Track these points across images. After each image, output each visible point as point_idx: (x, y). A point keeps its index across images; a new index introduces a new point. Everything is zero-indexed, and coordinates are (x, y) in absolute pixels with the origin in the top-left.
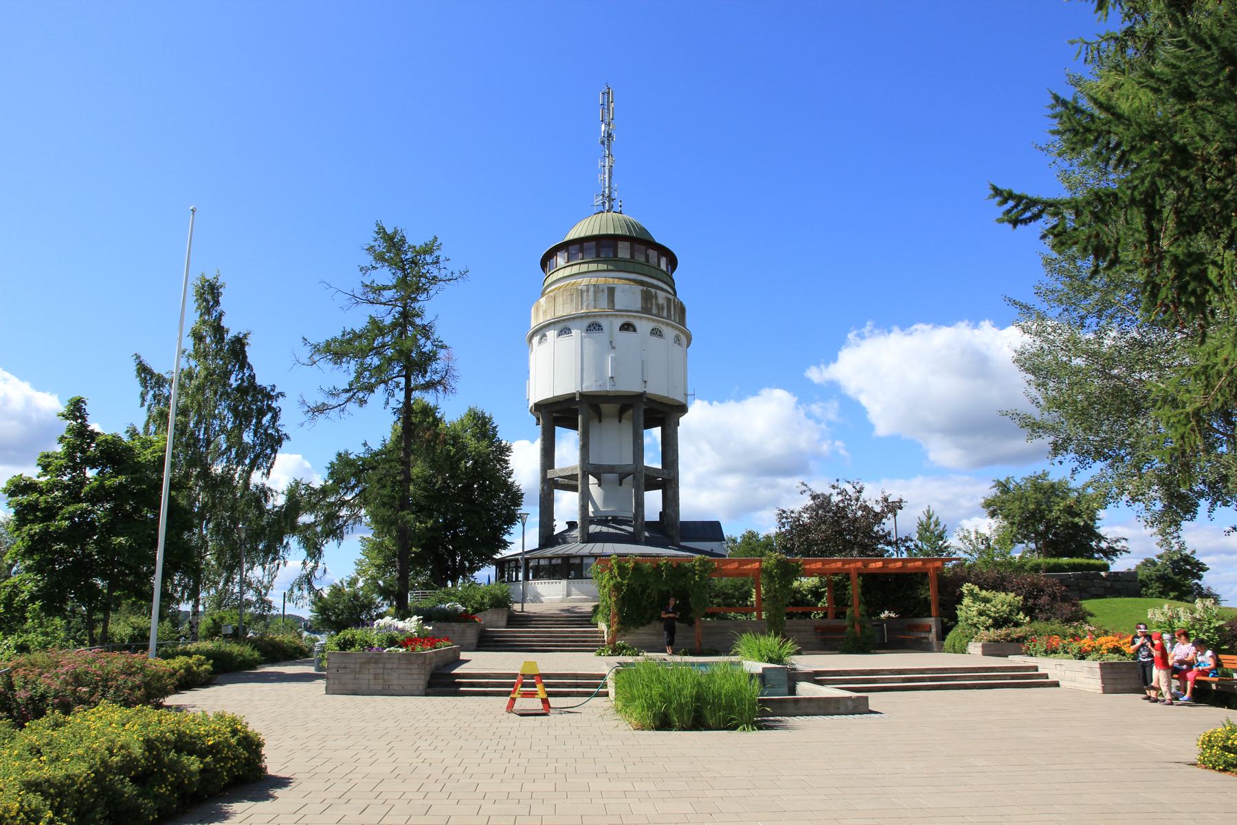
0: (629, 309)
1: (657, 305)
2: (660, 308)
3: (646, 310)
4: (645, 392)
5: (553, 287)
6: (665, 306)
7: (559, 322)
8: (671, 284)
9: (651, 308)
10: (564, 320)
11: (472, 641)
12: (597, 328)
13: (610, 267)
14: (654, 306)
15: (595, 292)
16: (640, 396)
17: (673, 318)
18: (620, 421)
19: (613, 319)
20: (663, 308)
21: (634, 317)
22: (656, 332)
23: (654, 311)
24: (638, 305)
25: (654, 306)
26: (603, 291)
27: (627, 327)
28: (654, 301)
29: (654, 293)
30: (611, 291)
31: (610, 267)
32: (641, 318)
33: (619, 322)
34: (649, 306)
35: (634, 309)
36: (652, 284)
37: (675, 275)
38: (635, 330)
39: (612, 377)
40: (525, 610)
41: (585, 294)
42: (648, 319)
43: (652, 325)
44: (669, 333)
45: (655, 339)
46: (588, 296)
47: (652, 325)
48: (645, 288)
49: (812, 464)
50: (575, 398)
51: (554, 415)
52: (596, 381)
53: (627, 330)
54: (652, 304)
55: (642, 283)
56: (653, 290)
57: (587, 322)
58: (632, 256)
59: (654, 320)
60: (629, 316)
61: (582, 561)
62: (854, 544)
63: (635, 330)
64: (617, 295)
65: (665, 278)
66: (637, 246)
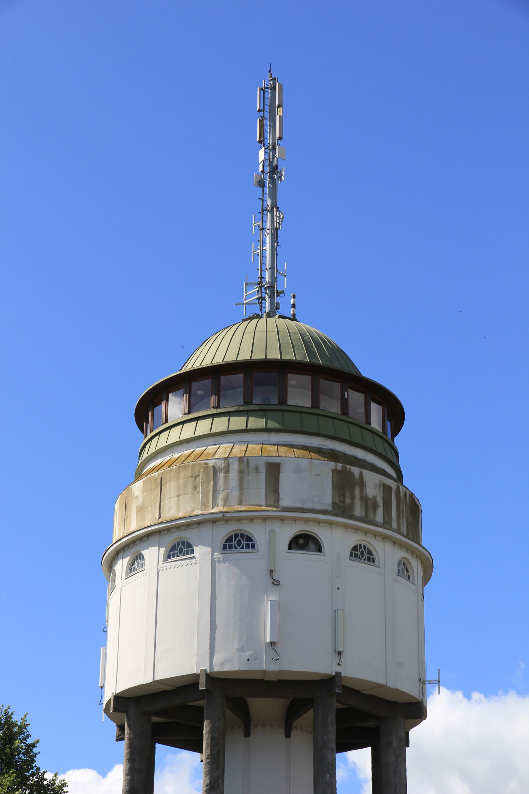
1: (364, 499)
4: (338, 674)
5: (159, 461)
6: (380, 500)
7: (168, 530)
9: (352, 505)
10: (178, 527)
12: (185, 550)
13: (272, 424)
14: (357, 502)
17: (395, 525)
18: (288, 735)
19: (277, 526)
20: (375, 506)
21: (319, 522)
23: (358, 511)
25: (357, 502)
28: (357, 492)
29: (357, 476)
31: (272, 424)
32: (331, 524)
34: (348, 501)
35: (318, 507)
38: (319, 549)
39: (272, 644)
42: (346, 527)
48: (340, 466)
50: (197, 684)
51: (155, 719)
53: (303, 547)
54: (353, 497)
56: (356, 471)
58: (315, 404)
59: (357, 529)
60: (307, 521)
63: (319, 549)
66: (323, 383)
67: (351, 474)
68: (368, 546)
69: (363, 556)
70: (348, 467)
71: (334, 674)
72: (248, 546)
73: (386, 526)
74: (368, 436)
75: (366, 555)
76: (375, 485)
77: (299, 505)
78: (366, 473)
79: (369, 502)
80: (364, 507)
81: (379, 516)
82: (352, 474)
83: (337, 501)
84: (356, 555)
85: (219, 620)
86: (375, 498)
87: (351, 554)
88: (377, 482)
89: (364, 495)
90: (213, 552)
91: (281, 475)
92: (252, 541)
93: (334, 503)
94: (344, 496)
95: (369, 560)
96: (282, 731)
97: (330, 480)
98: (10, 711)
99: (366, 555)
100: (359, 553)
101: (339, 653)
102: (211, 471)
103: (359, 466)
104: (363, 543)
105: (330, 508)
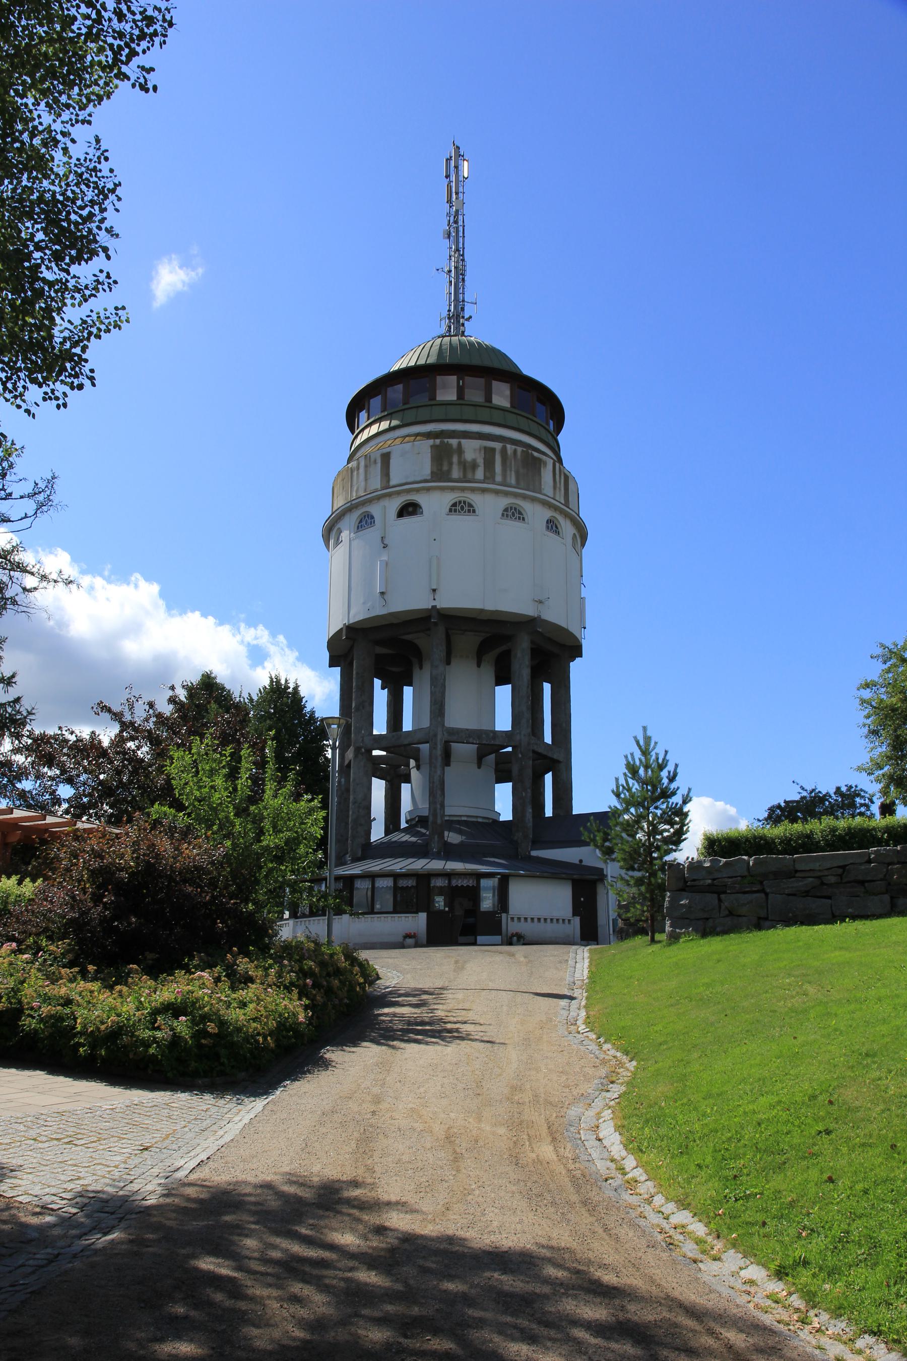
0: (409, 480)
2: (468, 467)
3: (440, 474)
4: (434, 607)
6: (481, 461)
8: (556, 450)
11: (587, 955)
13: (395, 423)
15: (366, 466)
16: (530, 624)
17: (499, 478)
19: (386, 502)
21: (418, 490)
22: (460, 508)
23: (456, 473)
24: (425, 468)
26: (375, 462)
27: (409, 510)
28: (455, 459)
30: (386, 458)
31: (395, 423)
33: (395, 504)
35: (418, 479)
36: (454, 431)
37: (561, 438)
39: (382, 593)
40: (716, 895)
41: (355, 473)
42: (442, 489)
43: (449, 498)
44: (537, 515)
45: (512, 525)
46: (358, 474)
47: (449, 498)
48: (438, 441)
49: (246, 643)
52: (364, 603)
54: (451, 464)
55: (428, 435)
56: (454, 442)
57: (355, 516)
59: (453, 489)
61: (478, 883)
62: (280, 887)
64: (394, 462)
65: (550, 439)
67: (449, 446)
68: (468, 500)
69: (514, 516)
70: (446, 440)
71: (430, 607)
72: (469, 511)
73: (486, 481)
74: (543, 431)
75: (554, 528)
76: (475, 450)
77: (404, 481)
78: (464, 442)
79: (467, 464)
80: (462, 470)
81: (480, 474)
82: (451, 445)
83: (435, 470)
84: (507, 516)
85: (353, 585)
86: (474, 461)
87: (503, 515)
88: (478, 447)
89: (462, 460)
90: (350, 534)
91: (391, 461)
92: (472, 507)
93: (432, 473)
94: (441, 465)
95: (519, 518)
96: (475, 662)
97: (429, 455)
98: (879, 651)
99: (554, 528)
100: (550, 526)
101: (434, 590)
102: (350, 471)
103: (453, 438)
104: (462, 499)
105: (429, 478)
